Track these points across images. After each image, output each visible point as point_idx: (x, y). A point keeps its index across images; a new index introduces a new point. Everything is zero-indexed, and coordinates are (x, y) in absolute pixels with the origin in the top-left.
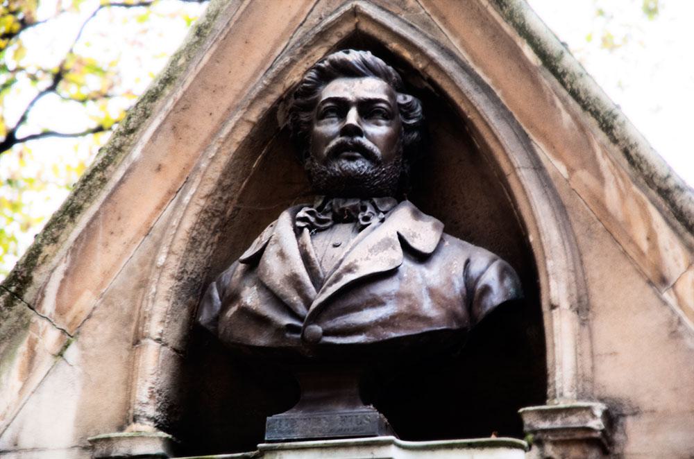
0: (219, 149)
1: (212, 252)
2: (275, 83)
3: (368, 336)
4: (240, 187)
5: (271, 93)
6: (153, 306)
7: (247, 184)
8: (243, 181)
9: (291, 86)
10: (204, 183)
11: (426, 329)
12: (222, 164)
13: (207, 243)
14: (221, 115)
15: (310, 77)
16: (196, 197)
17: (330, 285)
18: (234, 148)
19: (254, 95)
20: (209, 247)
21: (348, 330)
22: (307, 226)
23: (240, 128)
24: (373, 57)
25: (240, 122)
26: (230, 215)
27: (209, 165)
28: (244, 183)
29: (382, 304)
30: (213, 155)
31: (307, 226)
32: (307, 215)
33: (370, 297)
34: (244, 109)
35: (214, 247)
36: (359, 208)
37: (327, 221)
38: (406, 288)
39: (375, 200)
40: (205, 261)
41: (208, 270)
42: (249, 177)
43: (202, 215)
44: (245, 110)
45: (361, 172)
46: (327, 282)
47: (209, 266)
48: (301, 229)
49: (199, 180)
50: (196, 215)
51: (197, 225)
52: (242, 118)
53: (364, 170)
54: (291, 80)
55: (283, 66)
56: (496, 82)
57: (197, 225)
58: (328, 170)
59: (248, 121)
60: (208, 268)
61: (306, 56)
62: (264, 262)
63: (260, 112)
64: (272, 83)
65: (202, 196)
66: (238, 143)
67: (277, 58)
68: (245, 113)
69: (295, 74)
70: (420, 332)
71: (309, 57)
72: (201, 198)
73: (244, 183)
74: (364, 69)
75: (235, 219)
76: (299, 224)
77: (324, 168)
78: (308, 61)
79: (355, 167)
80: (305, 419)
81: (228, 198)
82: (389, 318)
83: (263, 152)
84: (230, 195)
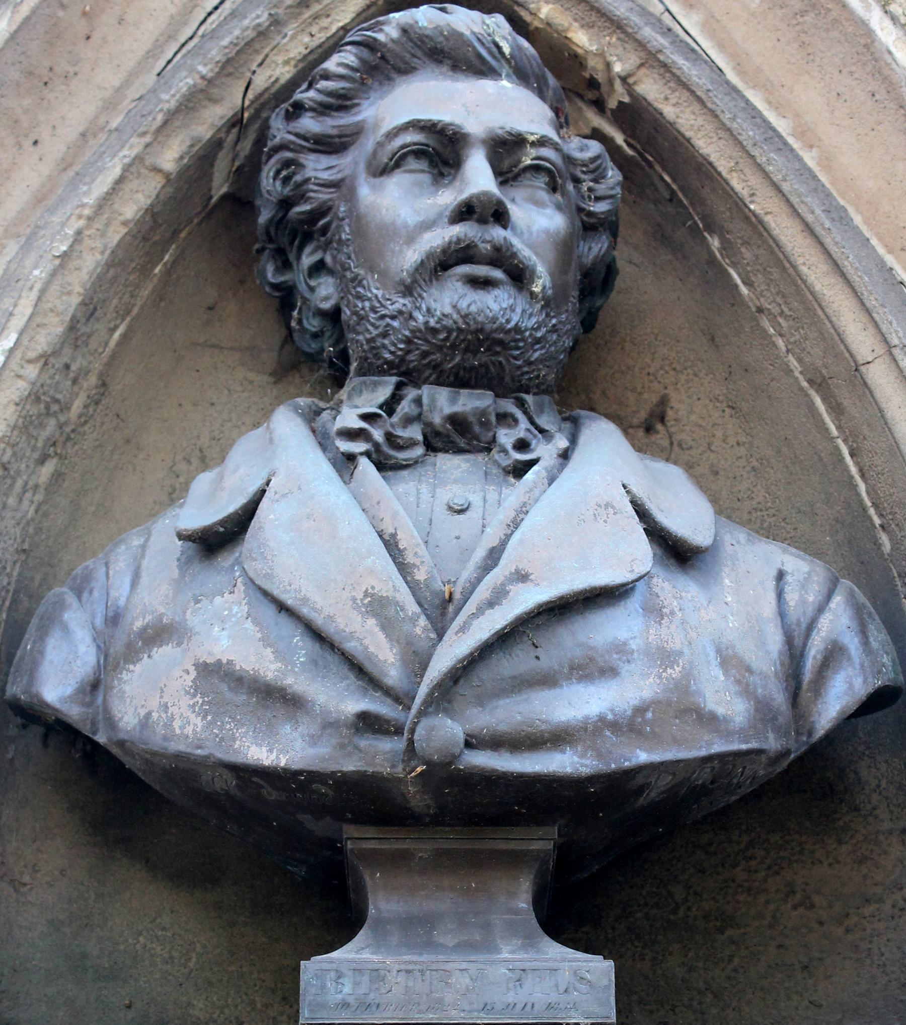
0: (79, 233)
1: (32, 509)
2: (230, 75)
3: (582, 756)
4: (106, 344)
5: (214, 101)
6: (451, 687)
7: (124, 337)
8: (114, 329)
9: (267, 89)
10: (38, 320)
11: (719, 747)
12: (84, 275)
13: (26, 483)
14: (64, 149)
15: (340, 64)
16: (18, 354)
17: (480, 611)
18: (116, 235)
19: (169, 99)
20: (28, 495)
21: (528, 736)
22: (367, 454)
23: (133, 184)
24: (514, 34)
25: (133, 169)
26: (80, 417)
27: (53, 274)
28: (117, 335)
29: (609, 672)
30: (64, 248)
31: (367, 454)
32: (363, 425)
33: (578, 652)
34: (144, 134)
35: (39, 497)
36: (493, 419)
37: (411, 444)
38: (677, 643)
39: (529, 398)
40: (18, 531)
41: (23, 557)
42: (128, 319)
43: (28, 407)
44: (148, 139)
45: (508, 321)
46: (470, 607)
47: (26, 546)
48: (351, 458)
49: (29, 311)
50: (17, 404)
51: (15, 433)
52: (138, 159)
53: (515, 318)
54: (268, 73)
55: (251, 34)
56: (801, 133)
57: (15, 433)
58: (419, 308)
59: (156, 170)
60: (24, 551)
61: (307, 14)
62: (760, 541)
63: (184, 148)
64: (218, 74)
65: (32, 355)
66: (125, 223)
67: (210, 14)
68: (147, 146)
69: (280, 59)
70: (703, 753)
71: (316, 17)
72: (30, 361)
73: (117, 335)
74: (494, 57)
75: (86, 428)
76: (345, 446)
77: (401, 303)
78: (314, 29)
79: (495, 307)
80: (408, 972)
81: (80, 369)
82: (629, 713)
83: (167, 257)
84: (85, 363)
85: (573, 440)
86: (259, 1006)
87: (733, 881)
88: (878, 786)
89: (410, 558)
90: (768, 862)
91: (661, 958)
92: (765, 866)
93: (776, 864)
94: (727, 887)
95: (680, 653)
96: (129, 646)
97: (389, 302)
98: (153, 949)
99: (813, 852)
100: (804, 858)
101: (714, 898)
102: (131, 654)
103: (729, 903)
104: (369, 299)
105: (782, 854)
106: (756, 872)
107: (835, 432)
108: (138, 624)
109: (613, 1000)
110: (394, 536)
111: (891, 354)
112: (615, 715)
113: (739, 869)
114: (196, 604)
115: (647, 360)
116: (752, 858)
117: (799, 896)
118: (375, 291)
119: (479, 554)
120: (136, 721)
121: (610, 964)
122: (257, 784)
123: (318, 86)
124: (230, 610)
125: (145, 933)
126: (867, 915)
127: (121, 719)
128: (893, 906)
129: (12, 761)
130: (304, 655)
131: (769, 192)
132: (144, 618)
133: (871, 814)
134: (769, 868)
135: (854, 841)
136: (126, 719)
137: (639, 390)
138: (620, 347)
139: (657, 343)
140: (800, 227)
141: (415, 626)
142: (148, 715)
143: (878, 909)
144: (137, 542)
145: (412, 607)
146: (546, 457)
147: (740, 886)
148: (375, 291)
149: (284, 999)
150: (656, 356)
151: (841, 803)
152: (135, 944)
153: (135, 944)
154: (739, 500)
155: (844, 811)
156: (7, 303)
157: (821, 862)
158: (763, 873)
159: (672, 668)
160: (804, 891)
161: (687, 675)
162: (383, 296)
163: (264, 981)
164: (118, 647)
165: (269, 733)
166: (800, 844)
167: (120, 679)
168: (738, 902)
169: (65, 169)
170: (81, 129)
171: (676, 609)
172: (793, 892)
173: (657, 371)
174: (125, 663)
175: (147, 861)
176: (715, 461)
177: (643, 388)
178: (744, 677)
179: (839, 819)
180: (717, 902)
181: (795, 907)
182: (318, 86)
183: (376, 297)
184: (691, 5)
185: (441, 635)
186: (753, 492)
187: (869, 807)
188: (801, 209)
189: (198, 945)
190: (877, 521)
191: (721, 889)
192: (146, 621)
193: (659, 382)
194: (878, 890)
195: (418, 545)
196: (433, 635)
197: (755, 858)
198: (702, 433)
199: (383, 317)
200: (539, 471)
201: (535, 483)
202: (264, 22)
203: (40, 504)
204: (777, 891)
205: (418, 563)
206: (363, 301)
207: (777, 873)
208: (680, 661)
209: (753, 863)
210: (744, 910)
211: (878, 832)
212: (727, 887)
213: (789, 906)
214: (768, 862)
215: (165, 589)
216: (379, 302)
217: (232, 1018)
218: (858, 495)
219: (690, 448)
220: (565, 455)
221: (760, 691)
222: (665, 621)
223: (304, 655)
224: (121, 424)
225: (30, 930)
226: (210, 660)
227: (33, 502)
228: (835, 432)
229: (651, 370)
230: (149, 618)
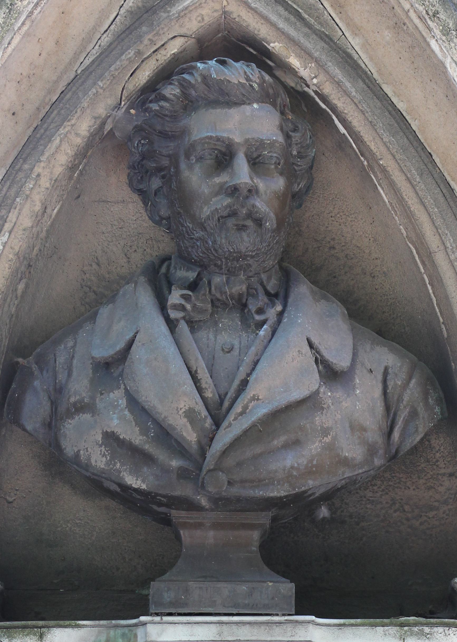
28: (56, 211)
31: (184, 318)
85: (285, 306)
86: (127, 560)
87: (365, 497)
88: (439, 450)
89: (204, 386)
90: (383, 487)
91: (327, 537)
92: (381, 489)
93: (387, 489)
94: (361, 500)
95: (331, 428)
96: (68, 410)
97: (195, 232)
98: (75, 530)
99: (405, 483)
100: (401, 486)
101: (355, 506)
102: (69, 414)
103: (362, 508)
104: (185, 227)
105: (391, 483)
106: (377, 492)
107: (423, 271)
108: (72, 400)
109: (293, 602)
110: (196, 371)
111: (446, 251)
112: (298, 464)
113: (368, 490)
114: (101, 395)
115: (331, 209)
116: (375, 485)
117: (397, 505)
118: (188, 224)
119: (237, 382)
120: (73, 453)
121: (293, 585)
122: (131, 492)
123: (160, 104)
124: (118, 402)
125: (71, 522)
126: (431, 516)
127: (65, 448)
128: (444, 513)
129: (4, 435)
130: (153, 433)
131: (390, 157)
132: (75, 397)
133: (435, 465)
134: (383, 490)
135: (426, 478)
136: (67, 449)
137: (326, 225)
138: (317, 201)
139: (336, 199)
140: (404, 178)
141: (205, 423)
142: (79, 451)
143: (436, 514)
144: (70, 344)
145: (204, 413)
146: (271, 318)
147: (369, 500)
148: (188, 224)
149: (140, 557)
150: (336, 206)
151: (420, 457)
152: (66, 528)
153: (66, 528)
154: (376, 289)
155: (422, 462)
156: (4, 212)
157: (409, 488)
158: (381, 493)
159: (327, 437)
160: (400, 503)
161: (335, 438)
162: (192, 228)
163: (130, 547)
164: (62, 409)
165: (136, 472)
166: (400, 478)
167: (64, 426)
168: (367, 508)
169: (29, 127)
170: (37, 105)
171: (330, 404)
172: (394, 503)
173: (336, 215)
174: (66, 418)
175: (72, 485)
176: (364, 267)
177: (328, 224)
178: (362, 435)
179: (419, 466)
180: (357, 508)
181: (395, 511)
182: (160, 104)
183: (189, 227)
184: (356, 34)
185: (218, 429)
186: (383, 285)
187: (434, 460)
188: (405, 169)
189: (97, 528)
190: (441, 320)
191: (359, 501)
192: (77, 399)
193: (337, 221)
194: (436, 504)
195: (207, 378)
196: (214, 427)
197: (377, 485)
198: (359, 251)
199: (192, 238)
200: (267, 329)
201: (264, 337)
202: (132, 56)
203: (18, 305)
204: (387, 503)
205: (207, 387)
206: (182, 226)
207: (387, 494)
208: (331, 433)
209: (375, 488)
210: (370, 512)
211: (438, 474)
212: (361, 500)
213: (392, 511)
214: (383, 487)
215: (86, 382)
216: (190, 230)
217: (114, 566)
218: (433, 303)
219: (352, 259)
220: (281, 314)
221: (370, 439)
222: (325, 412)
223: (153, 433)
224: (57, 250)
225: (14, 522)
226: (109, 430)
227: (15, 304)
228: (423, 271)
229: (333, 215)
230: (78, 397)
